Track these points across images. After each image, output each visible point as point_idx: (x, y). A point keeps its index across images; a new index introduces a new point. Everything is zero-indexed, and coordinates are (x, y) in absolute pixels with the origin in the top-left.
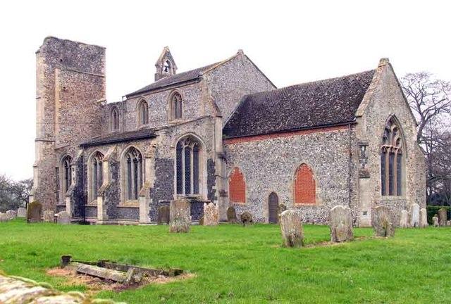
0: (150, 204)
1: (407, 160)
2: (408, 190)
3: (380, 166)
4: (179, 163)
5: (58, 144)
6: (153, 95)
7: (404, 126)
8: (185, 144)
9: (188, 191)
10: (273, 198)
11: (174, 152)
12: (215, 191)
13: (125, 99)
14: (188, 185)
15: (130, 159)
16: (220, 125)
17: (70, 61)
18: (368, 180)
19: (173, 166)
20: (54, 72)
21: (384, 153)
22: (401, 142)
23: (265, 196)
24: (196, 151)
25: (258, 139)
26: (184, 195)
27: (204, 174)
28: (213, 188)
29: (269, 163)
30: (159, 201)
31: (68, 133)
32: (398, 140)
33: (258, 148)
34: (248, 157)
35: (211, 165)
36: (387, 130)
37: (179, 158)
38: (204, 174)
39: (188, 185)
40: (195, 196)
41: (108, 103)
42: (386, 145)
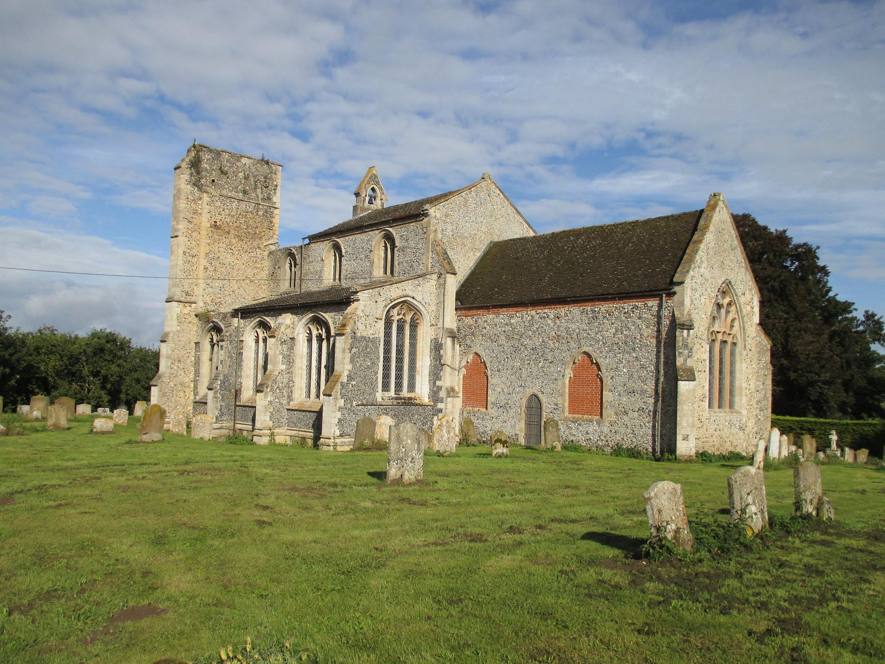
0: (340, 409)
1: (744, 353)
2: (744, 400)
3: (708, 361)
4: (387, 343)
5: (200, 307)
6: (351, 237)
7: (742, 300)
8: (398, 315)
9: (399, 386)
10: (534, 405)
11: (381, 325)
12: (440, 388)
13: (307, 241)
14: (399, 377)
15: (310, 333)
16: (453, 284)
17: (785, 231)
18: (692, 384)
19: (377, 348)
20: (200, 199)
21: (713, 340)
22: (736, 324)
23: (520, 401)
24: (414, 326)
25: (512, 311)
26: (392, 393)
27: (424, 362)
28: (438, 383)
29: (595, 367)
30: (354, 403)
31: (217, 290)
32: (733, 320)
33: (511, 324)
34: (494, 339)
35: (437, 347)
36: (719, 306)
37: (388, 335)
38: (424, 362)
39: (399, 377)
40: (411, 395)
41: (281, 247)
42: (716, 329)
